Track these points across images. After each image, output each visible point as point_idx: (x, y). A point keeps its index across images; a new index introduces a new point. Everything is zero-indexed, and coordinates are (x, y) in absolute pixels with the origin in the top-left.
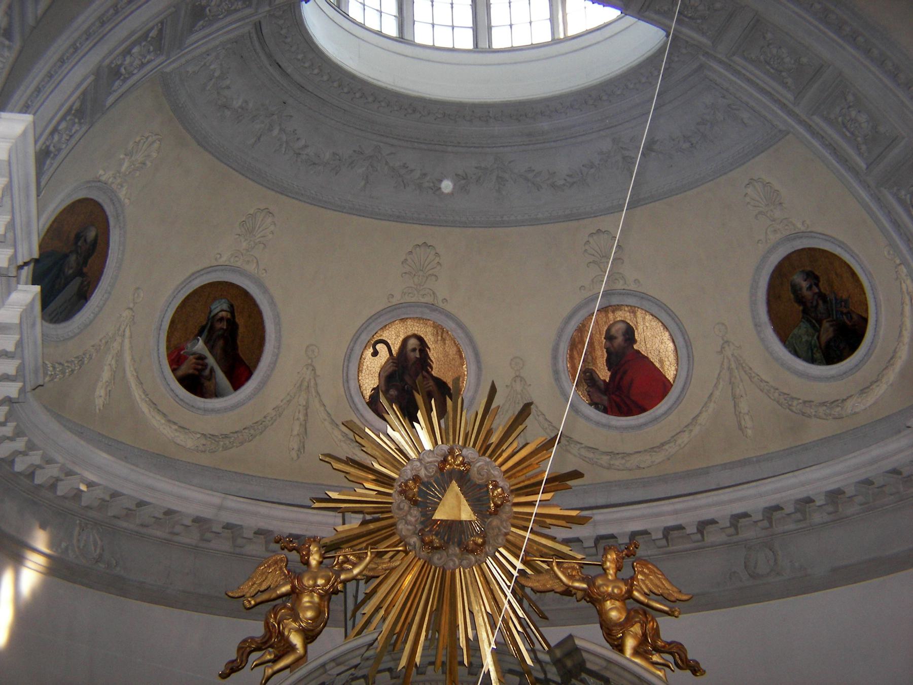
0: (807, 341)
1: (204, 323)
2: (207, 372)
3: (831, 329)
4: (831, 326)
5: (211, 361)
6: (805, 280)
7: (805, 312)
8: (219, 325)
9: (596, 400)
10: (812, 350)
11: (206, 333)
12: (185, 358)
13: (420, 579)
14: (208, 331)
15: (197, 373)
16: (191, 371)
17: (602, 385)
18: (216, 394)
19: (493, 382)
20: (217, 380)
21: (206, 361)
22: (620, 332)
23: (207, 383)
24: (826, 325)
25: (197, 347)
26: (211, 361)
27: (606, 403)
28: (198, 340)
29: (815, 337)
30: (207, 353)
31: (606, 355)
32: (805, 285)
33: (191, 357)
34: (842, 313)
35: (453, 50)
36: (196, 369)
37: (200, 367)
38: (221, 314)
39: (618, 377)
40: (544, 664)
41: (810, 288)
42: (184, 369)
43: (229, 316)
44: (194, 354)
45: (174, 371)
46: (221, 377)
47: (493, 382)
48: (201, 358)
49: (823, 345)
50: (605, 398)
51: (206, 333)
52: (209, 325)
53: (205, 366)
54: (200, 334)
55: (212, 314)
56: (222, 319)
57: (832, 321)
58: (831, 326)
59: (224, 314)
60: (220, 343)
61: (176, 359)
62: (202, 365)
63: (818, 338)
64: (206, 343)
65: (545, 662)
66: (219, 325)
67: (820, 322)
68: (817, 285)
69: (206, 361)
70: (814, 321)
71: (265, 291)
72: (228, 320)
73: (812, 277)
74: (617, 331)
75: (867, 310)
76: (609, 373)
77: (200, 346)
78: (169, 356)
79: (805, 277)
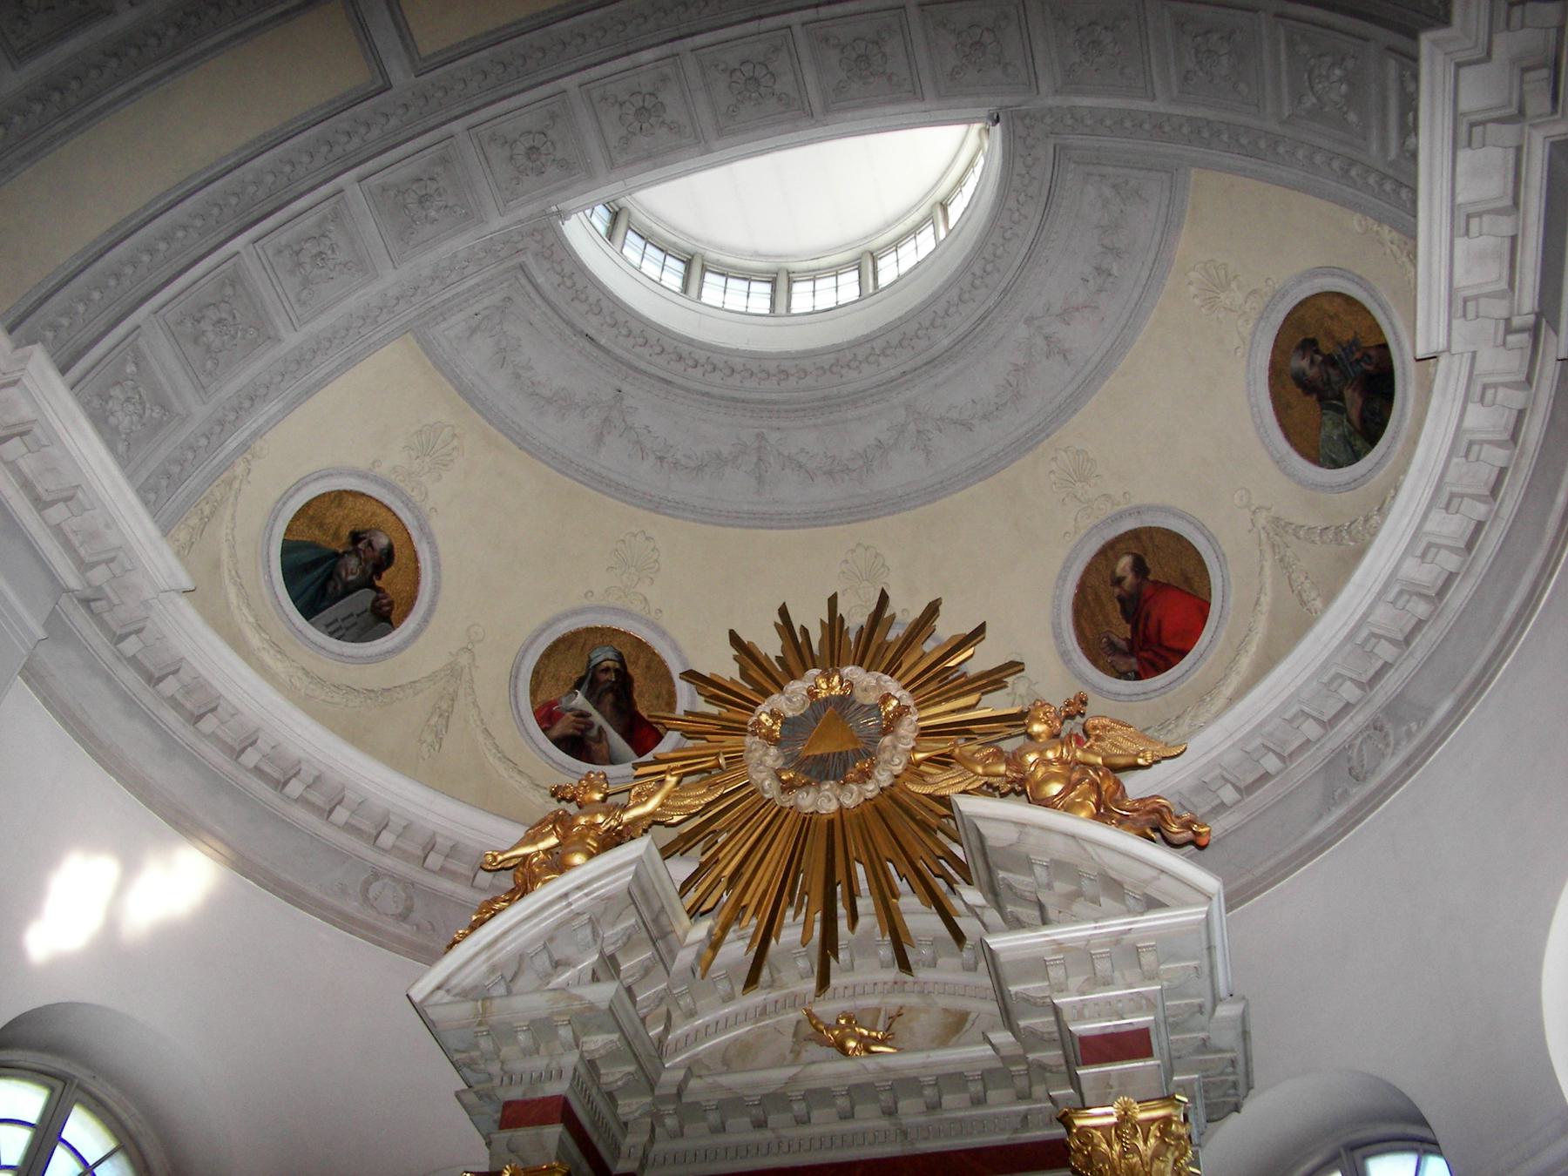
0: (1339, 435)
1: (583, 674)
2: (594, 733)
3: (1356, 394)
4: (1354, 390)
5: (597, 718)
6: (1304, 358)
7: (1320, 399)
8: (603, 677)
9: (1124, 668)
10: (1349, 443)
11: (585, 686)
12: (560, 715)
13: (799, 847)
14: (590, 682)
15: (579, 733)
16: (571, 731)
17: (1123, 644)
18: (612, 760)
19: (883, 590)
20: (610, 742)
21: (591, 719)
22: (1128, 568)
23: (595, 747)
24: (1348, 393)
25: (574, 703)
26: (597, 718)
27: (1136, 667)
28: (576, 694)
29: (1345, 422)
30: (589, 708)
31: (1118, 606)
32: (1305, 363)
33: (568, 714)
34: (1358, 361)
35: (839, 307)
36: (578, 729)
37: (582, 726)
38: (605, 664)
39: (1141, 627)
40: (978, 910)
41: (1312, 362)
42: (559, 729)
43: (618, 666)
44: (571, 710)
45: (544, 730)
46: (616, 739)
47: (883, 590)
48: (583, 715)
49: (1359, 428)
50: (1133, 660)
51: (585, 686)
52: (590, 675)
53: (591, 725)
54: (578, 685)
55: (593, 663)
56: (607, 670)
57: (1352, 384)
58: (1354, 390)
59: (610, 664)
60: (610, 698)
61: (547, 716)
62: (586, 723)
63: (1349, 420)
64: (588, 696)
65: (979, 907)
66: (603, 677)
67: (1341, 398)
68: (1317, 352)
69: (591, 719)
70: (1335, 402)
71: (663, 634)
72: (616, 670)
73: (1309, 346)
74: (1124, 569)
75: (1381, 333)
76: (1129, 626)
77: (580, 700)
78: (536, 713)
79: (1301, 353)
